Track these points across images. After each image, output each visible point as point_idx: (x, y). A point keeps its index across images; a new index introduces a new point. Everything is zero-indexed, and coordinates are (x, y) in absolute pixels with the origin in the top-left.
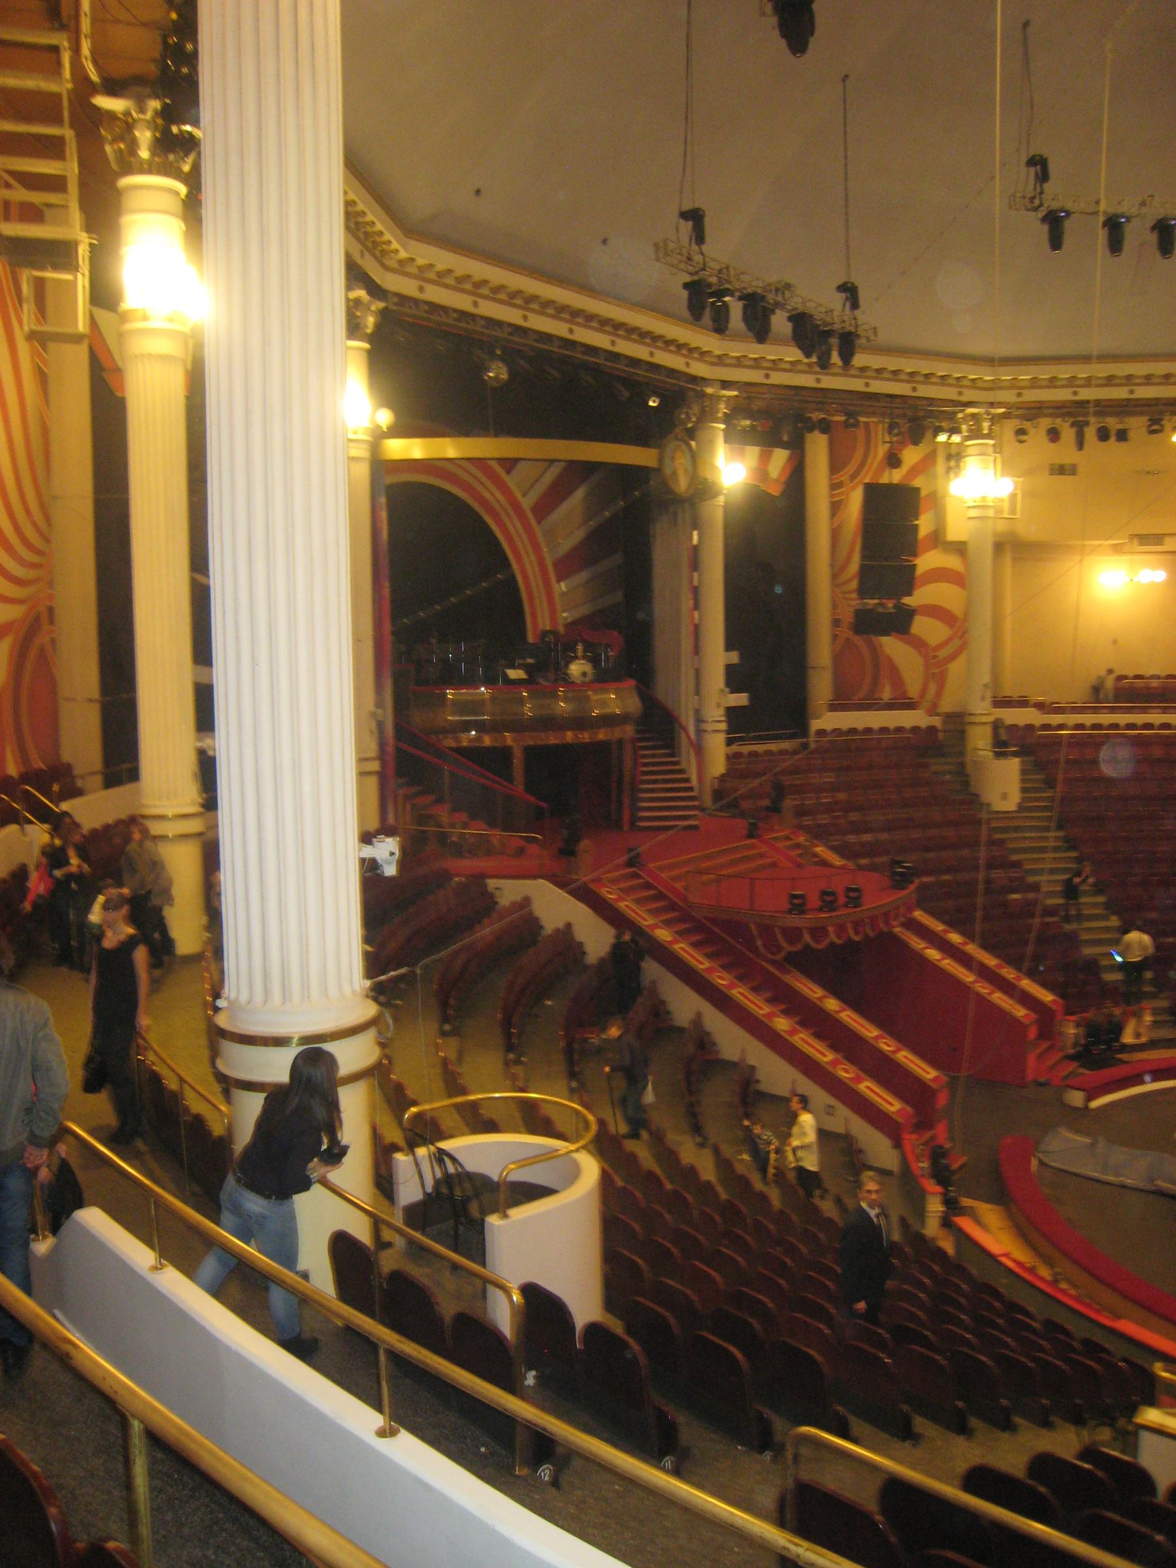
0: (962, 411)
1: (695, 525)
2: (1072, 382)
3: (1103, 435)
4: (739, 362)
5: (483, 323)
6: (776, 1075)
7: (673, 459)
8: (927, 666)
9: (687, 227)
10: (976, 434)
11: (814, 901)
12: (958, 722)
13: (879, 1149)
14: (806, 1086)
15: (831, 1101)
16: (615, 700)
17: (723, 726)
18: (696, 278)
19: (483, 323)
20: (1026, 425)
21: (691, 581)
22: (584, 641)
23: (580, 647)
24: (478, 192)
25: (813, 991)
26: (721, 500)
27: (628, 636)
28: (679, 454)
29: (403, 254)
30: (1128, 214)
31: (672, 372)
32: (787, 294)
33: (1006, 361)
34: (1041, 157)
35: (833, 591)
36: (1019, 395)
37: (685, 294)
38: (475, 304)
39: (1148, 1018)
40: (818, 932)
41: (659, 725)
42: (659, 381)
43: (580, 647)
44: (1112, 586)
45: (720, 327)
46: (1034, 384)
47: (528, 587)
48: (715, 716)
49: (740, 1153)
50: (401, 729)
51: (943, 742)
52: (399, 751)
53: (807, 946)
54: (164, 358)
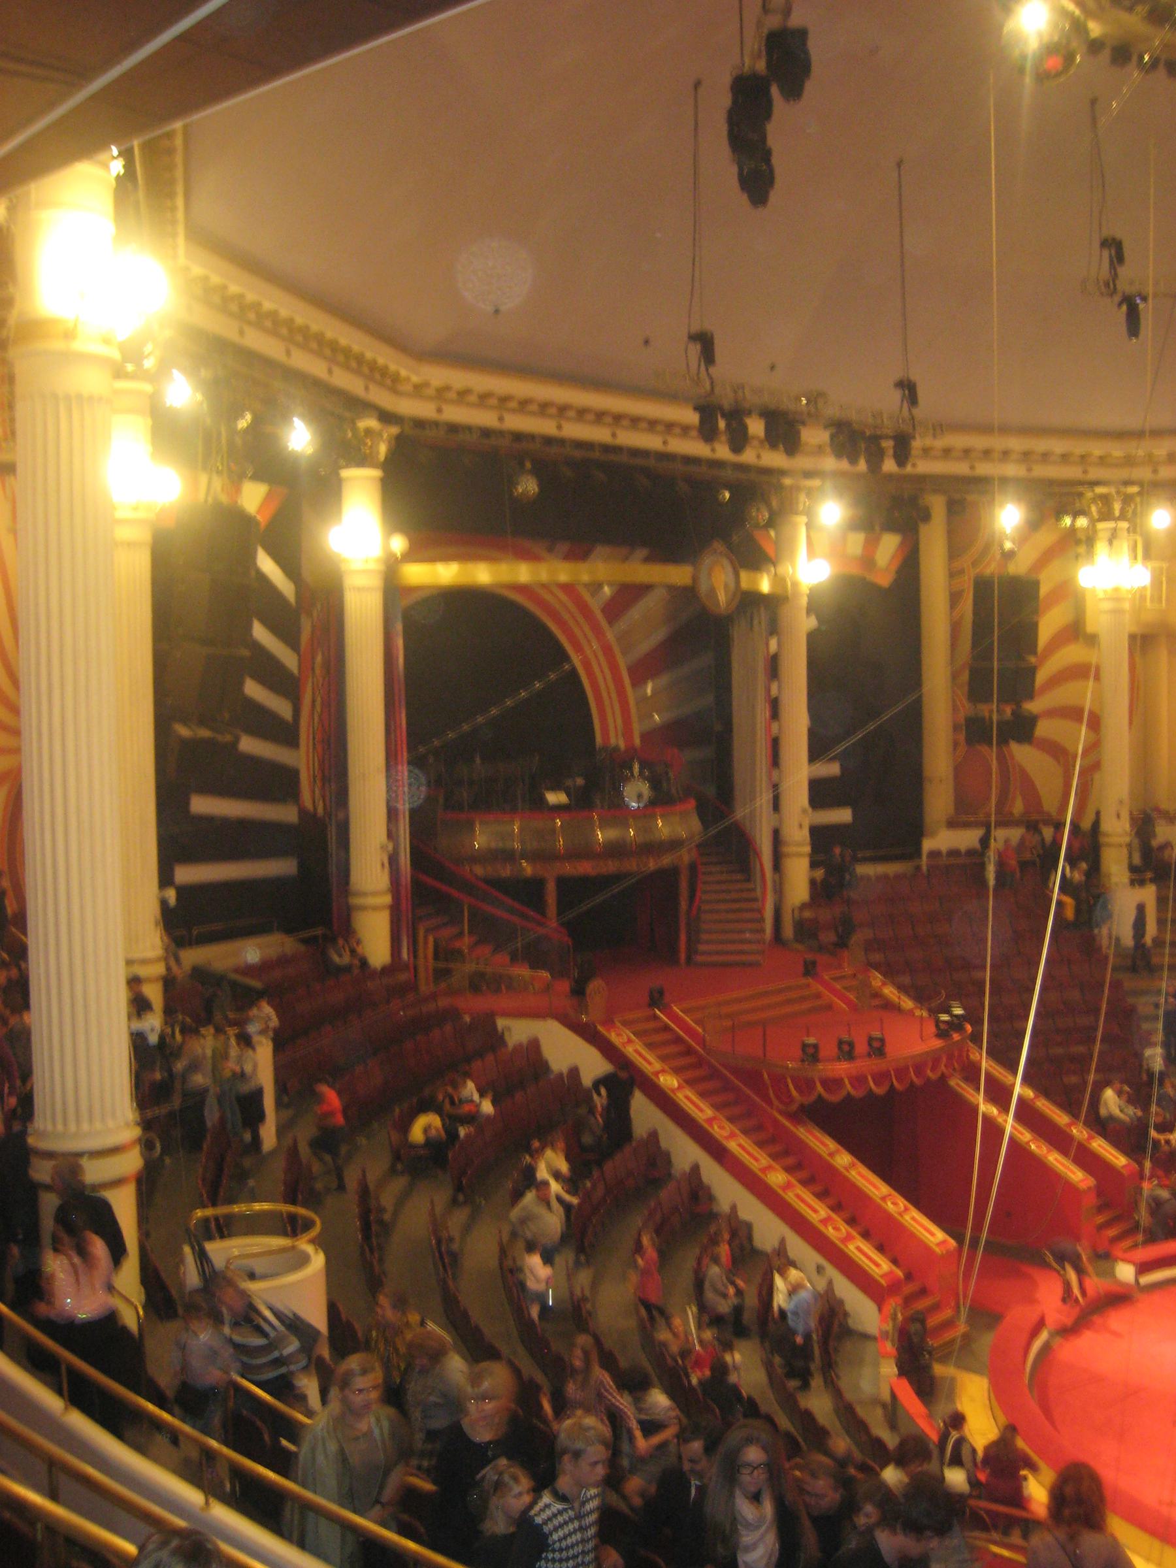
6: (768, 1230)
9: (695, 349)
10: (1107, 516)
11: (861, 1048)
13: (865, 1313)
17: (807, 849)
21: (768, 690)
23: (636, 767)
25: (823, 1145)
27: (705, 754)
32: (820, 405)
34: (1114, 239)
35: (954, 692)
41: (730, 847)
43: (636, 767)
48: (798, 837)
50: (419, 857)
52: (416, 883)
53: (820, 1096)
54: (131, 545)
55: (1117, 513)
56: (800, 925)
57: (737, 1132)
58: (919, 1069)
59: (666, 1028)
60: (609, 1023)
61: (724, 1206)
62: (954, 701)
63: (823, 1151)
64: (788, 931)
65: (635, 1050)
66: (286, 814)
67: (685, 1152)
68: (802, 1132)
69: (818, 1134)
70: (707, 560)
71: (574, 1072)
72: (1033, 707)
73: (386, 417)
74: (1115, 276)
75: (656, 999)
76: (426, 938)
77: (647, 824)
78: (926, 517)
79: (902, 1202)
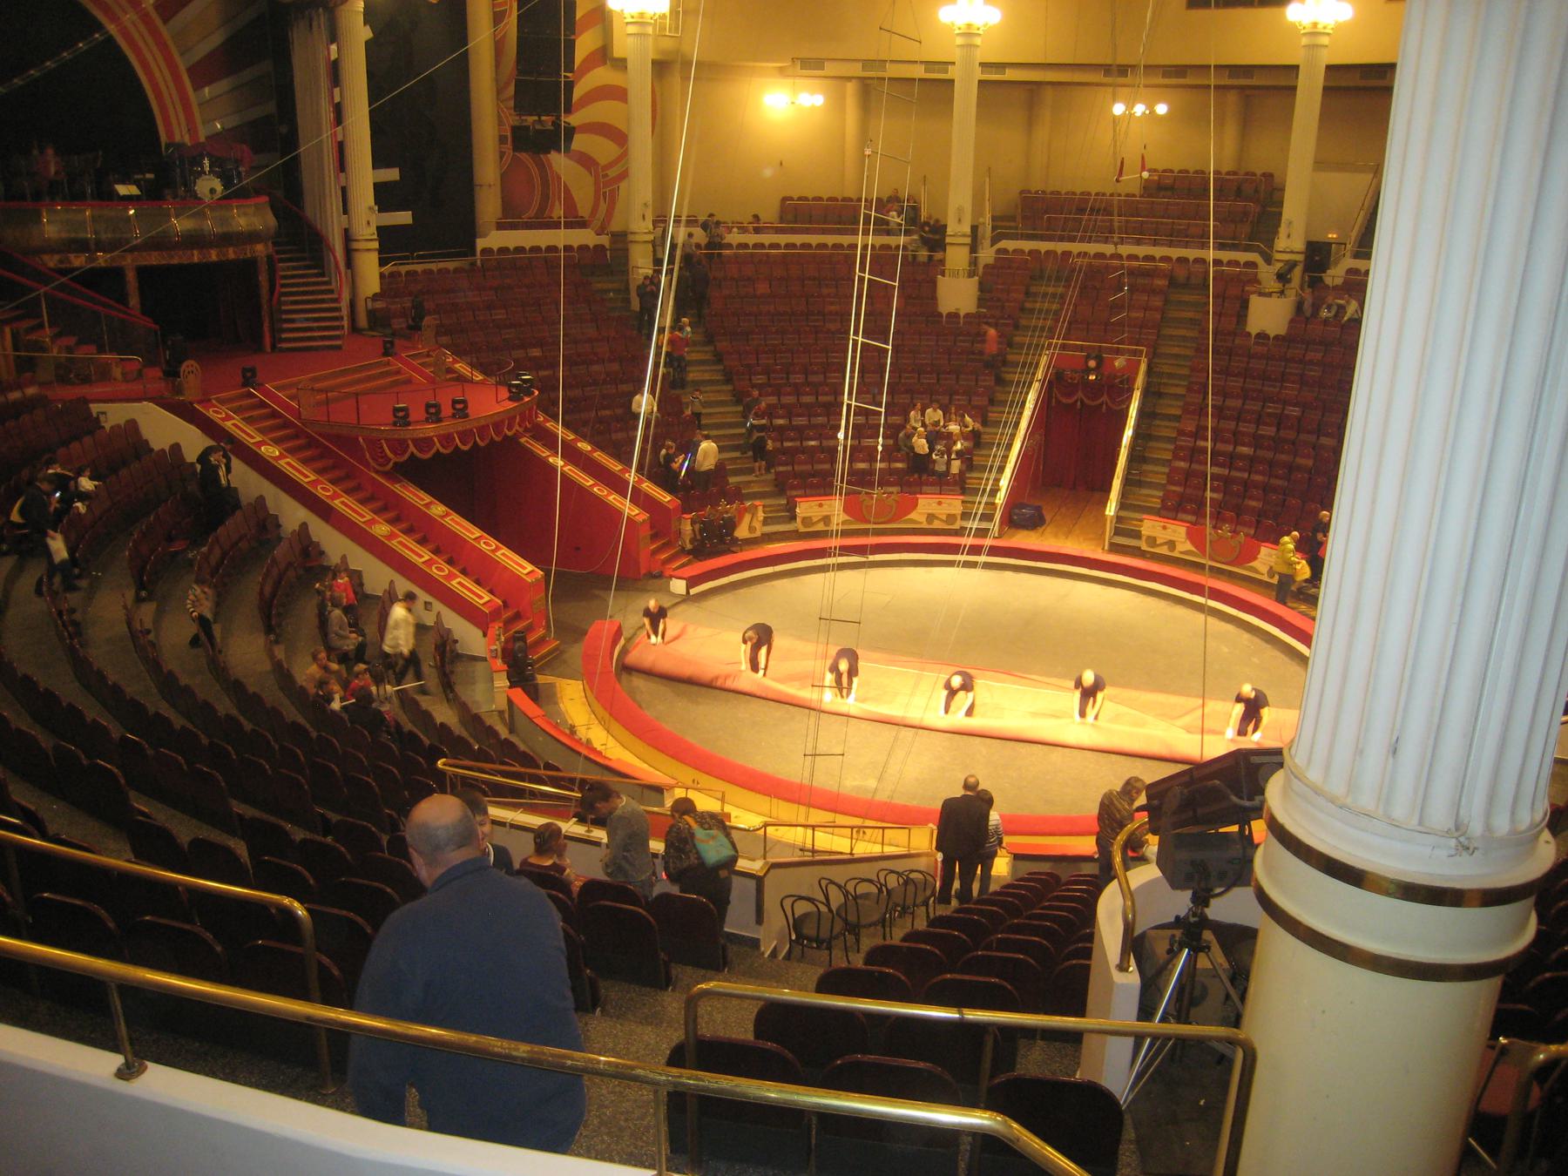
1: (333, 38)
6: (378, 576)
8: (596, 183)
11: (447, 410)
12: (622, 240)
13: (471, 639)
14: (403, 585)
15: (429, 599)
16: (251, 218)
17: (376, 245)
22: (210, 156)
25: (418, 498)
35: (499, 107)
39: (761, 515)
41: (301, 238)
47: (159, 95)
51: (608, 260)
56: (371, 314)
58: (498, 426)
59: (263, 405)
60: (206, 401)
61: (334, 559)
63: (420, 504)
64: (363, 321)
65: (233, 425)
67: (293, 515)
71: (176, 448)
72: (574, 120)
75: (249, 378)
77: (220, 215)
79: (494, 543)
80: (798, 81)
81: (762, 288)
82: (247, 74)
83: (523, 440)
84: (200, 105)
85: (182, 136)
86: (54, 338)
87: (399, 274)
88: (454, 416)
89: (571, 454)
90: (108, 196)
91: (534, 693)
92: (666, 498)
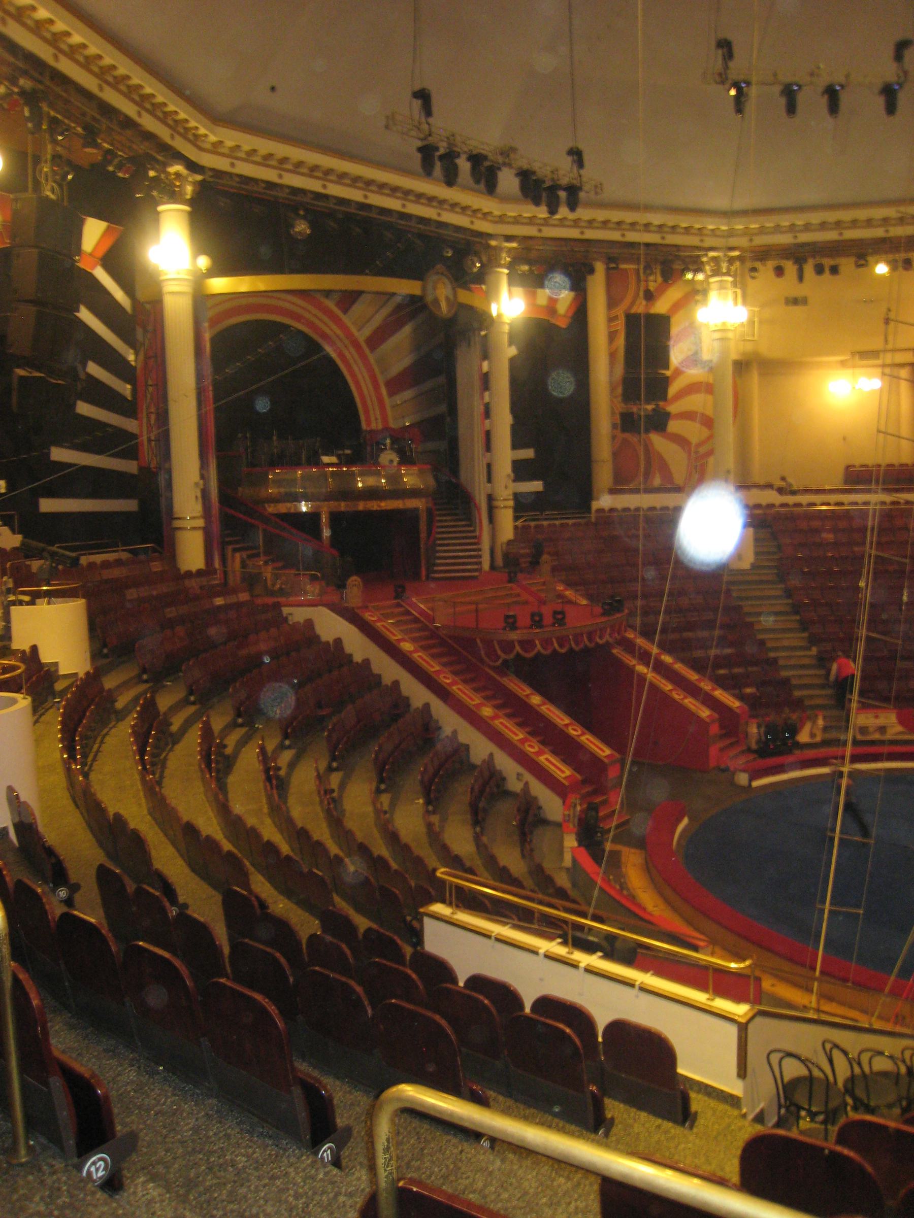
0: (706, 255)
1: (485, 356)
2: (792, 228)
3: (819, 270)
4: (517, 221)
5: (263, 185)
7: (435, 289)
9: (417, 103)
10: (717, 272)
11: (548, 619)
13: (552, 805)
18: (425, 143)
19: (263, 185)
20: (758, 264)
24: (273, 89)
25: (523, 690)
26: (506, 329)
27: (439, 437)
28: (440, 285)
29: (213, 138)
30: (801, 83)
31: (458, 229)
33: (744, 213)
35: (612, 401)
36: (751, 240)
37: (419, 156)
38: (233, 165)
39: (820, 722)
40: (527, 644)
41: (454, 499)
42: (431, 231)
43: (388, 441)
44: (844, 394)
45: (450, 179)
46: (762, 231)
49: (418, 799)
55: (724, 271)
56: (506, 556)
57: (459, 681)
62: (612, 408)
64: (499, 562)
66: (130, 467)
68: (505, 681)
69: (516, 682)
70: (432, 278)
73: (193, 167)
74: (726, 67)
76: (233, 557)
77: (394, 479)
78: (592, 271)
80: (857, 371)
81: (829, 537)
82: (428, 385)
83: (615, 651)
84: (393, 407)
85: (376, 424)
86: (266, 563)
87: (529, 527)
88: (554, 625)
89: (660, 668)
90: (317, 463)
91: (597, 854)
92: (735, 704)
